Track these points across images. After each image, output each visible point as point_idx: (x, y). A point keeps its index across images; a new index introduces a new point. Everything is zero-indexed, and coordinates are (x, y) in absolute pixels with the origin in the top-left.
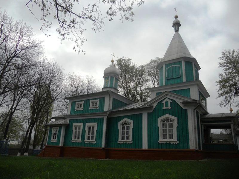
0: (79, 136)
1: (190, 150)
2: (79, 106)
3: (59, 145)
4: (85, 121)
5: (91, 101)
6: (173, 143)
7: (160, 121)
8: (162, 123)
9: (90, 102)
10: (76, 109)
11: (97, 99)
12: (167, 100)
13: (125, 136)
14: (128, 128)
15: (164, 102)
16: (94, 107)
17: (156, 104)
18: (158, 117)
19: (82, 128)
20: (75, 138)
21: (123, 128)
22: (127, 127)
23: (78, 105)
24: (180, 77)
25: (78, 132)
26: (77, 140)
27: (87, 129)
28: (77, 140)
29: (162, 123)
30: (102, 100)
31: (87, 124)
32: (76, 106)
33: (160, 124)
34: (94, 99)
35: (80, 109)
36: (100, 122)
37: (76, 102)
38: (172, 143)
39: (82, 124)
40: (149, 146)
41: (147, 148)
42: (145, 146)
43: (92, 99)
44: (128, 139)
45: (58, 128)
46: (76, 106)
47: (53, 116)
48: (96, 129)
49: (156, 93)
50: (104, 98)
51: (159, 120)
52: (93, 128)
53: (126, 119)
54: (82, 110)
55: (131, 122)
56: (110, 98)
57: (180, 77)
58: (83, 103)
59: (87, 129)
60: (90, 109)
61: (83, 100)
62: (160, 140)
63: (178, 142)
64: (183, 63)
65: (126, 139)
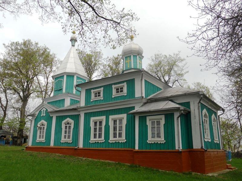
0: (43, 136)
1: (193, 150)
2: (98, 94)
3: (134, 148)
4: (107, 113)
5: (92, 91)
6: (160, 143)
7: (111, 119)
8: (65, 125)
9: (91, 92)
10: (92, 98)
11: (100, 87)
12: (44, 109)
13: (98, 133)
14: (70, 127)
15: (42, 111)
16: (97, 97)
17: (38, 112)
18: (62, 121)
19: (104, 124)
20: (40, 138)
21: (66, 127)
22: (69, 126)
23: (117, 89)
24: (61, 90)
25: (119, 127)
26: (97, 139)
27: (111, 124)
28: (118, 138)
29: (65, 125)
30: (131, 83)
31: (111, 117)
32: (114, 91)
33: (63, 126)
34: (96, 88)
35: (98, 98)
36: (76, 118)
37: (112, 84)
38: (159, 143)
39: (103, 118)
40: (183, 148)
41: (82, 147)
42: (81, 146)
43: (93, 89)
44: (100, 138)
45: (163, 117)
46: (114, 91)
47: (28, 114)
48: (104, 124)
49: (70, 99)
50: (133, 80)
51: (64, 122)
52: (101, 123)
53: (68, 120)
54: (126, 95)
55: (71, 121)
56: (142, 79)
57: (61, 90)
58: (102, 91)
59: (111, 124)
60: (92, 101)
61: (102, 86)
62: (110, 139)
63: (45, 141)
64: (65, 77)
65: (98, 138)
